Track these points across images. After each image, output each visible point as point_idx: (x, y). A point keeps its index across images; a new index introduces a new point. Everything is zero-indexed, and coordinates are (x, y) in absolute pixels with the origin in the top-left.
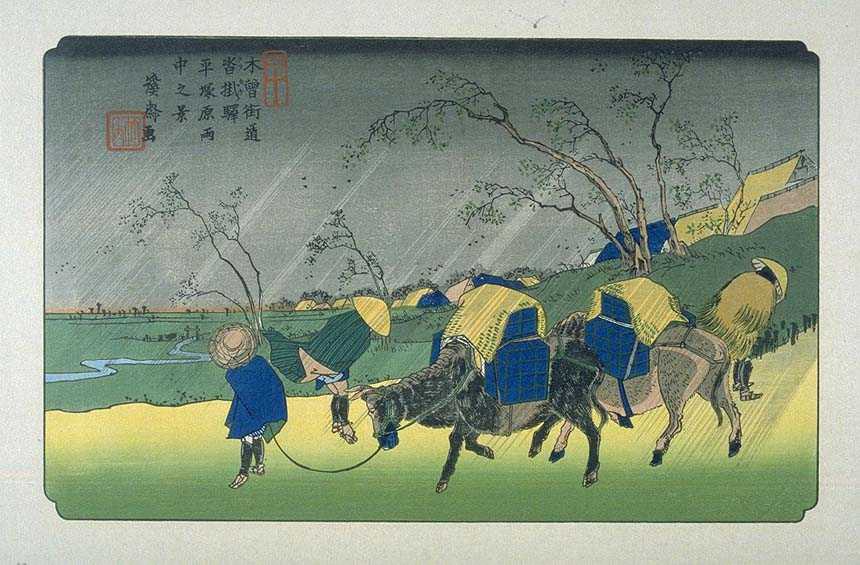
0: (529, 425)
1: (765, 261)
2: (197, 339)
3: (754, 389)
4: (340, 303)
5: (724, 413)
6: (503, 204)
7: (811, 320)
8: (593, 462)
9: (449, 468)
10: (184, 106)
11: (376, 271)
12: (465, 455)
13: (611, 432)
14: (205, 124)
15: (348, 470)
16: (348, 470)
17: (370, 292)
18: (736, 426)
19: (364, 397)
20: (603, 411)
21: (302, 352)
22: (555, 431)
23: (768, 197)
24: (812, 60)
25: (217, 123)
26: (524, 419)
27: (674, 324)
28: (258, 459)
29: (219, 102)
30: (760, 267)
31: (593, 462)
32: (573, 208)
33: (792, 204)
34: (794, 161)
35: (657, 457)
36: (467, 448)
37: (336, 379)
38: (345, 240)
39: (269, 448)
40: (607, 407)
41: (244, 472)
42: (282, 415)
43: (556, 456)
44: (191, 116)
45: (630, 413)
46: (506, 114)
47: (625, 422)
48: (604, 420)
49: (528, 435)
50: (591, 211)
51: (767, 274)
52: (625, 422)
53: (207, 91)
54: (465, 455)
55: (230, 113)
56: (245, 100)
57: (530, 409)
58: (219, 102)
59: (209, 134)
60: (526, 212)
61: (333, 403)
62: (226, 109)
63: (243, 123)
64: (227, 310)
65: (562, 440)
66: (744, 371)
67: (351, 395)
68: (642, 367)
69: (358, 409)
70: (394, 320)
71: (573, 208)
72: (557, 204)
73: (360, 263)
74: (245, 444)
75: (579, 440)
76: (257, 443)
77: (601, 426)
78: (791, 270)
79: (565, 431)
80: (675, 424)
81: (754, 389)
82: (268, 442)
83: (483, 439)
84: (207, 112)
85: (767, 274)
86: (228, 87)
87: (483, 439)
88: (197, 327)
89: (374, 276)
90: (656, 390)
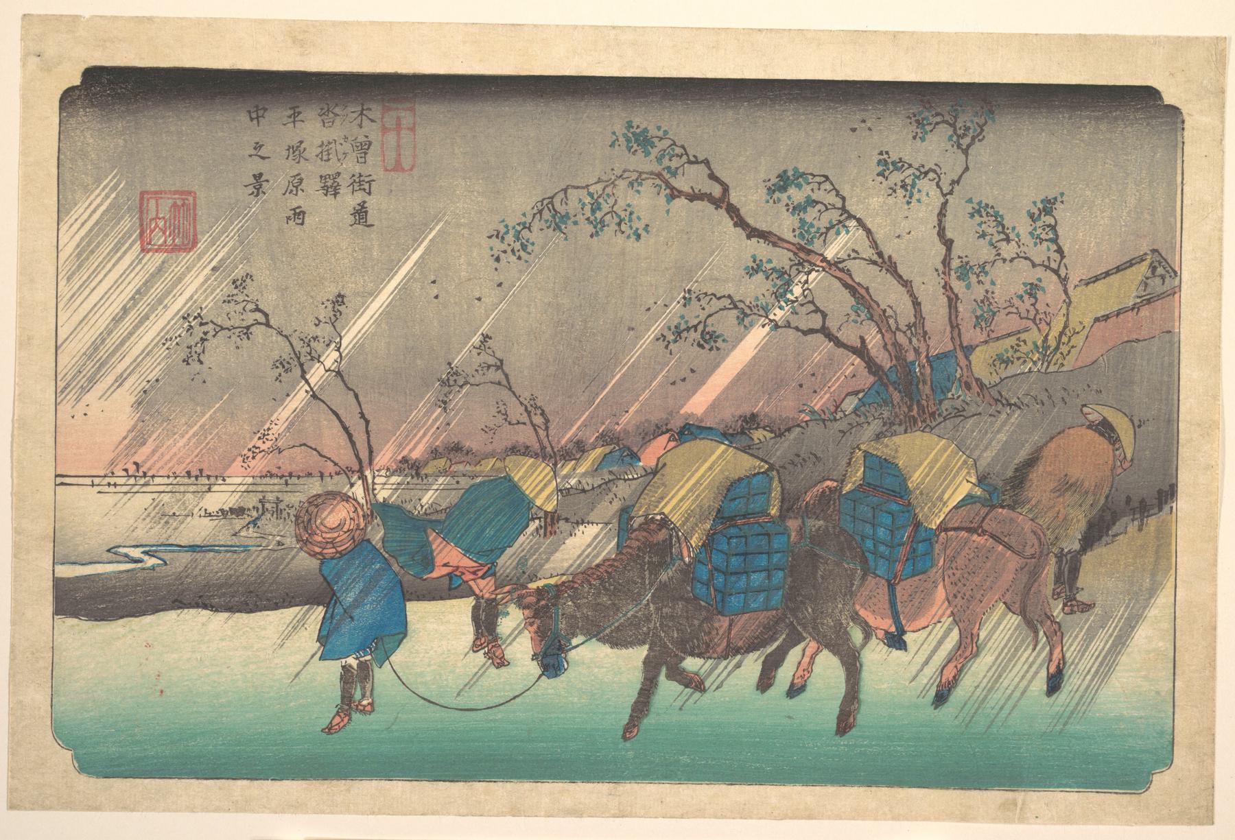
1: (1099, 408)
2: (245, 666)
6: (726, 323)
7: (1167, 494)
10: (261, 175)
12: (667, 689)
13: (875, 656)
17: (526, 451)
18: (1057, 654)
23: (1106, 317)
25: (311, 198)
26: (746, 625)
29: (312, 170)
32: (825, 331)
34: (1143, 268)
36: (669, 677)
39: (382, 675)
40: (872, 621)
43: (794, 691)
45: (902, 631)
46: (726, 189)
48: (867, 637)
49: (752, 665)
50: (849, 335)
52: (896, 641)
54: (667, 689)
55: (331, 187)
56: (350, 166)
61: (476, 609)
69: (511, 620)
71: (825, 331)
75: (828, 668)
76: (364, 668)
77: (864, 645)
79: (809, 652)
80: (968, 648)
84: (296, 185)
85: (1105, 429)
87: (691, 664)
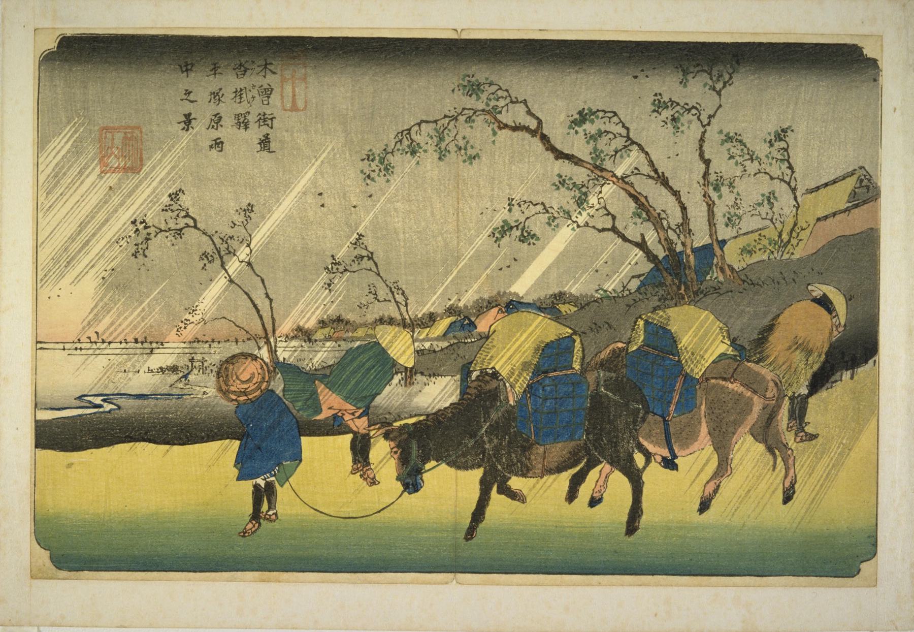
0: (559, 470)
3: (808, 429)
4: (360, 332)
5: (779, 459)
8: (636, 511)
9: (479, 514)
11: (400, 298)
14: (214, 134)
15: (379, 512)
16: (379, 512)
17: (391, 321)
19: (386, 436)
20: (648, 456)
21: (321, 388)
22: (593, 475)
24: (873, 64)
27: (723, 356)
28: (269, 502)
30: (817, 294)
31: (636, 511)
32: (614, 229)
33: (856, 222)
35: (471, 532)
37: (357, 414)
38: (366, 263)
39: (283, 493)
40: (651, 448)
41: (256, 515)
42: (297, 457)
43: (594, 502)
44: (199, 126)
45: (675, 456)
47: (670, 464)
49: (564, 479)
50: (633, 233)
51: (824, 302)
52: (670, 464)
53: (216, 96)
55: (242, 123)
57: (558, 450)
58: (228, 108)
59: (218, 144)
60: (565, 235)
62: (237, 116)
63: (255, 134)
64: (505, 229)
65: (601, 483)
66: (799, 412)
67: (372, 433)
68: (687, 405)
70: (419, 353)
71: (614, 229)
72: (618, 217)
73: (383, 293)
74: (256, 486)
75: (619, 484)
77: (644, 468)
78: (849, 299)
80: (723, 468)
81: (808, 429)
82: (282, 486)
83: (515, 483)
84: (217, 120)
85: (824, 302)
86: (238, 93)
87: (515, 483)
88: (203, 358)
89: (397, 302)
90: (704, 429)
